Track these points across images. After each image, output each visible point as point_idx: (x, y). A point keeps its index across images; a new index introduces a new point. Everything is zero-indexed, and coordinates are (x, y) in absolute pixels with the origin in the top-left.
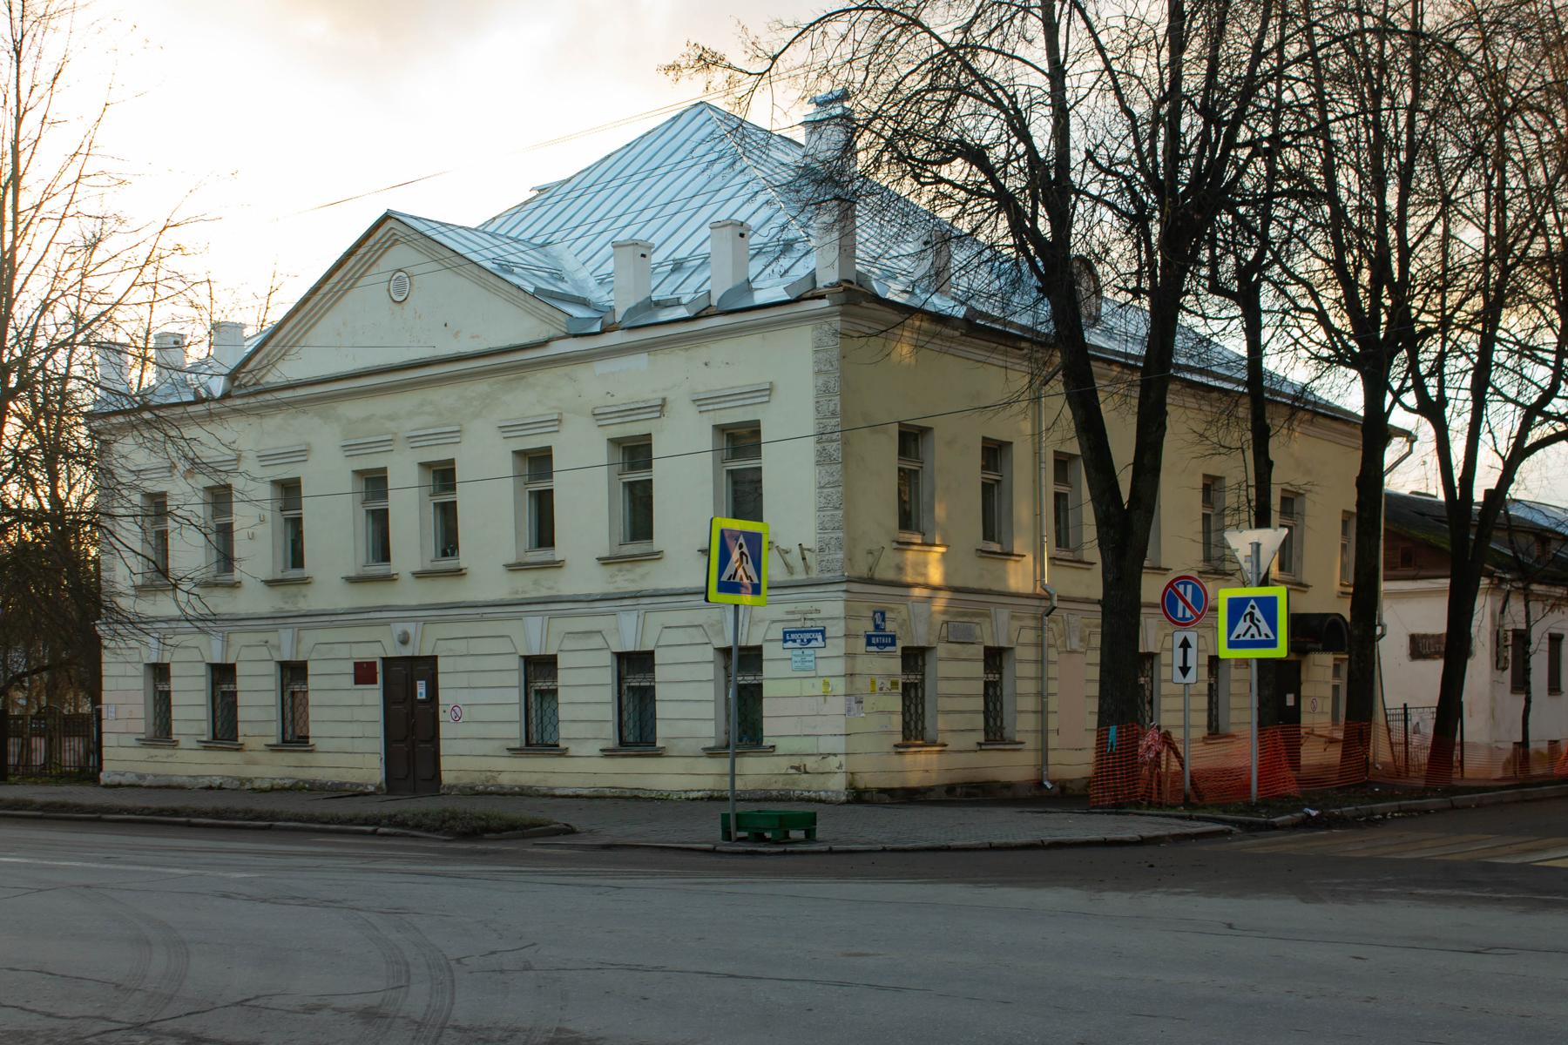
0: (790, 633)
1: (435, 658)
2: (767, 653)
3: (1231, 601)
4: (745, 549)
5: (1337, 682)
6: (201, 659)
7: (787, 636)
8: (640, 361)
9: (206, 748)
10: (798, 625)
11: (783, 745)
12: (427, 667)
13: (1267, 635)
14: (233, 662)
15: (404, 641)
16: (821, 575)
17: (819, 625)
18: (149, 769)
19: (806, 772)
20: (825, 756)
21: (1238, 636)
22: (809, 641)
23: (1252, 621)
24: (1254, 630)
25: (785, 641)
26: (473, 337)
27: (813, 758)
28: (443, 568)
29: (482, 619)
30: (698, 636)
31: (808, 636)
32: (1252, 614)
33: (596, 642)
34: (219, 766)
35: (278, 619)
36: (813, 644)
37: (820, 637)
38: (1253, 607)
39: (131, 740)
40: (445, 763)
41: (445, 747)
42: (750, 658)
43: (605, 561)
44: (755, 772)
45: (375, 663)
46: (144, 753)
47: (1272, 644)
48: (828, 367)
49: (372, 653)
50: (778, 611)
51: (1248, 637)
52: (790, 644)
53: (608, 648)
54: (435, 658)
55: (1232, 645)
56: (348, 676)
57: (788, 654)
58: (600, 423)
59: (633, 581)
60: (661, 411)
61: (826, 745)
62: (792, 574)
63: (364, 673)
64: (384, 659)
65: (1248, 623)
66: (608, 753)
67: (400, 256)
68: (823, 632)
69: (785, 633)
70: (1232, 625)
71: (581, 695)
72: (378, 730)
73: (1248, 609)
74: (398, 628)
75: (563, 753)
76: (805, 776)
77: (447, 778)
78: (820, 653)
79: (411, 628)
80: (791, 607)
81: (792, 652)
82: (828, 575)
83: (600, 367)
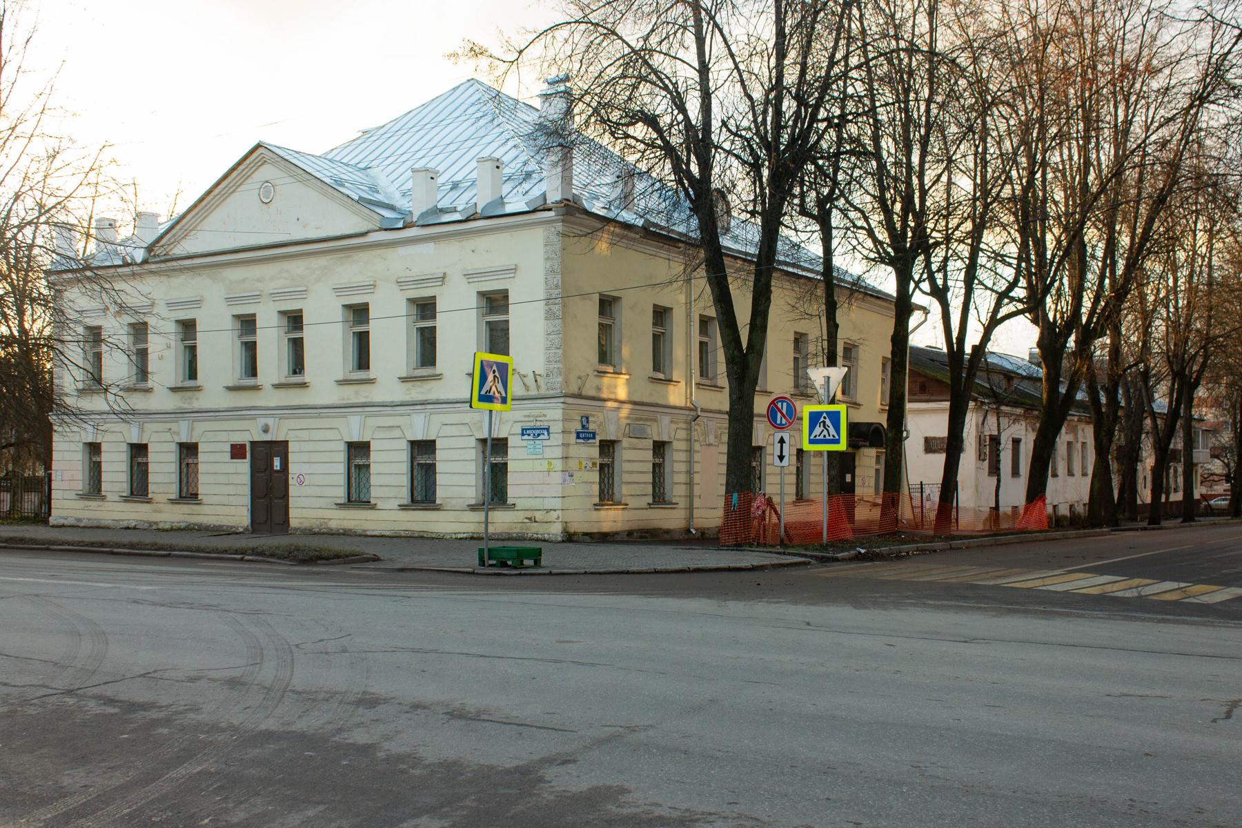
3: (811, 413)
4: (497, 374)
7: (524, 432)
8: (429, 247)
9: (125, 501)
11: (520, 504)
13: (834, 436)
15: (266, 431)
16: (547, 392)
17: (545, 424)
18: (80, 514)
19: (536, 522)
20: (548, 511)
21: (816, 436)
22: (539, 435)
23: (824, 426)
24: (825, 432)
25: (523, 435)
29: (319, 416)
31: (538, 432)
32: (824, 422)
33: (397, 433)
34: (135, 513)
35: (179, 414)
37: (546, 433)
38: (825, 418)
39: (72, 495)
42: (500, 445)
44: (502, 521)
45: (245, 445)
46: (82, 504)
47: (837, 442)
48: (553, 256)
49: (244, 438)
50: (519, 415)
51: (822, 437)
52: (526, 437)
53: (405, 438)
55: (811, 442)
57: (525, 443)
58: (471, 280)
61: (549, 504)
63: (237, 451)
64: (252, 443)
65: (822, 428)
66: (403, 508)
67: (266, 172)
68: (548, 429)
69: (523, 430)
72: (247, 490)
73: (822, 419)
74: (262, 421)
75: (374, 507)
77: (294, 523)
78: (546, 443)
79: (270, 422)
81: (527, 442)
82: (552, 392)
83: (402, 251)
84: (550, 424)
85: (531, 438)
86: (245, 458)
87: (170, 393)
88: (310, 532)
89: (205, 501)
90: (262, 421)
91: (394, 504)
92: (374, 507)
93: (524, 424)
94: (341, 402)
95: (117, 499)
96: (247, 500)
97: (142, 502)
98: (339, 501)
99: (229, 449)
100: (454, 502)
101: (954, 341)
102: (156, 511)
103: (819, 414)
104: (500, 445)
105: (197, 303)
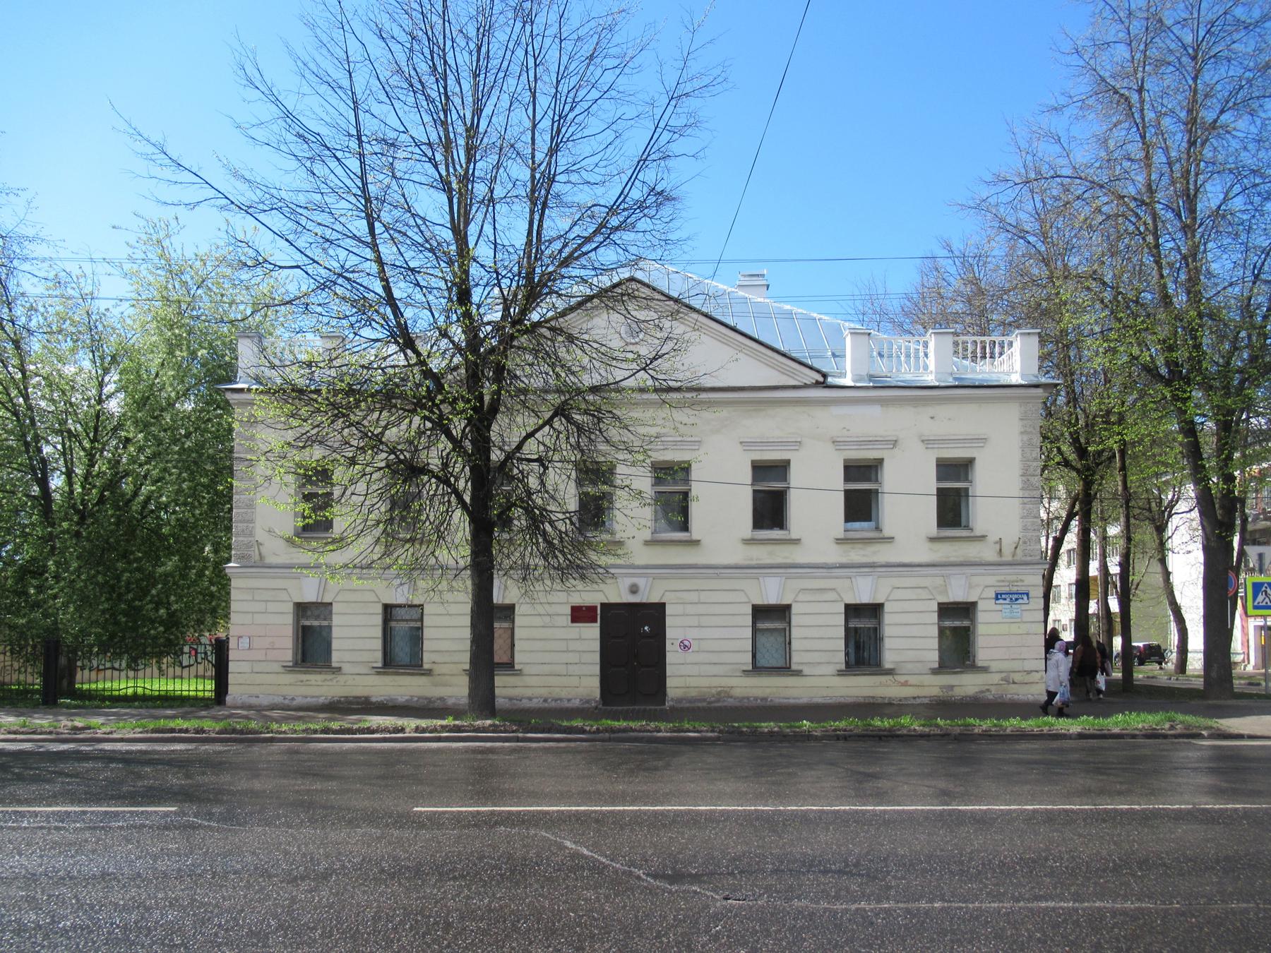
0: (1001, 594)
1: (663, 605)
2: (981, 606)
5: (408, 730)
6: (746, 600)
7: (998, 596)
8: (876, 410)
9: (378, 673)
10: (1007, 589)
11: (994, 666)
12: (324, 608)
14: (788, 603)
15: (634, 590)
16: (1024, 559)
17: (1023, 589)
18: (291, 691)
19: (1014, 683)
20: (1029, 672)
22: (1017, 599)
25: (997, 599)
26: (114, 227)
27: (1020, 674)
28: (668, 538)
29: (718, 577)
30: (924, 594)
31: (1016, 596)
32: (1266, 592)
33: (831, 596)
36: (1020, 601)
37: (1025, 597)
39: (277, 667)
40: (670, 682)
41: (670, 670)
42: (966, 610)
43: (839, 541)
44: (967, 684)
45: (595, 608)
46: (290, 678)
48: (1031, 429)
50: (991, 580)
52: (1001, 601)
53: (887, 600)
54: (663, 605)
56: (564, 617)
57: (999, 607)
59: (864, 555)
60: (894, 446)
61: (1029, 665)
62: (1001, 556)
64: (602, 604)
66: (840, 673)
68: (1027, 594)
69: (997, 595)
70: (1255, 598)
71: (444, 646)
72: (596, 658)
75: (798, 673)
76: (1013, 686)
78: (1024, 607)
79: (641, 582)
80: (1002, 578)
81: (1004, 606)
82: (1029, 559)
83: (836, 410)
84: (1029, 588)
85: (1007, 602)
86: (596, 622)
87: (929, 545)
88: (680, 700)
89: (527, 670)
90: (629, 581)
91: (831, 669)
92: (520, 673)
93: (997, 589)
94: (944, 559)
95: (281, 670)
96: (596, 669)
97: (417, 674)
98: (745, 668)
99: (569, 611)
100: (909, 666)
101: (1238, 529)
102: (436, 685)
103: (1262, 584)
104: (966, 610)
105: (982, 441)
